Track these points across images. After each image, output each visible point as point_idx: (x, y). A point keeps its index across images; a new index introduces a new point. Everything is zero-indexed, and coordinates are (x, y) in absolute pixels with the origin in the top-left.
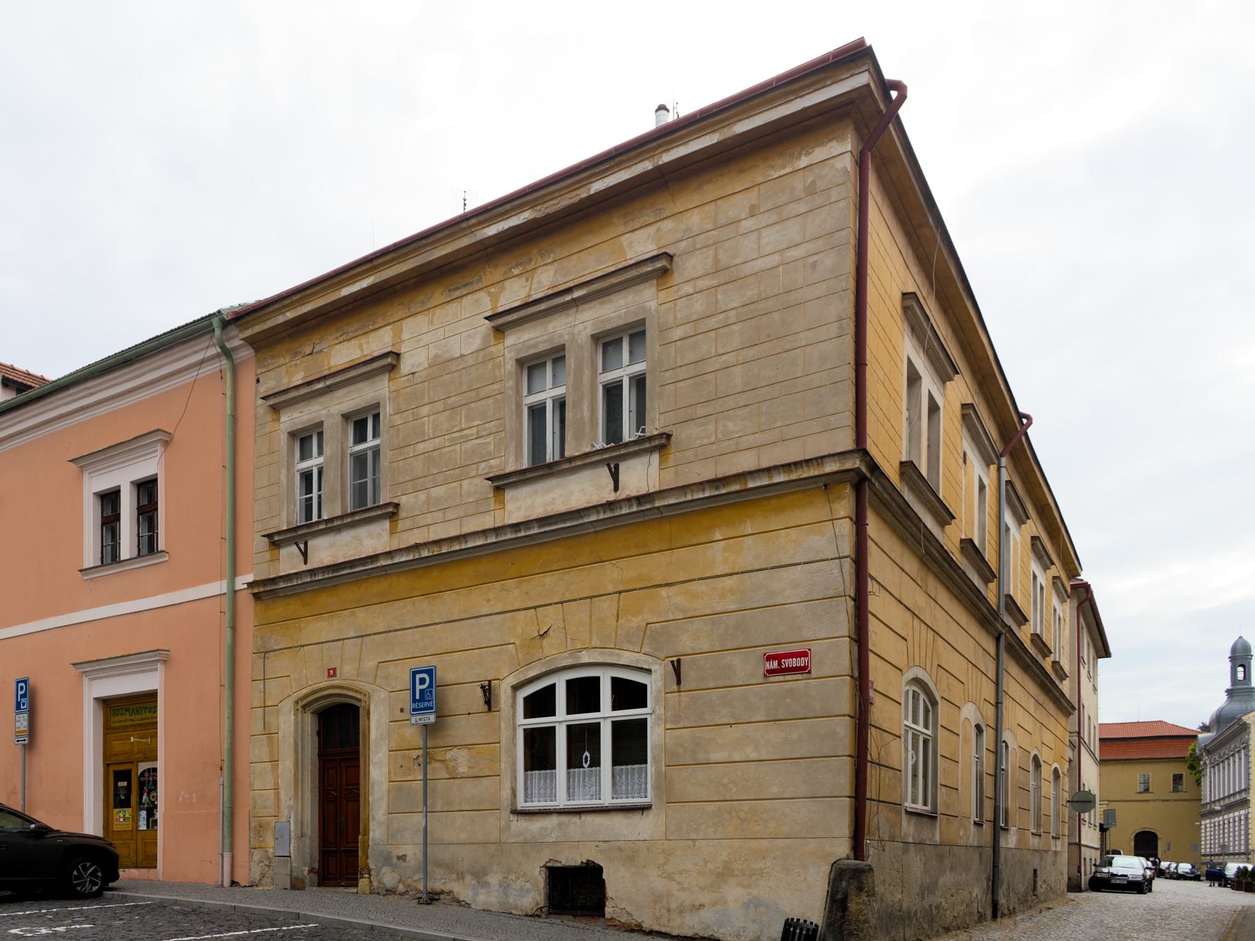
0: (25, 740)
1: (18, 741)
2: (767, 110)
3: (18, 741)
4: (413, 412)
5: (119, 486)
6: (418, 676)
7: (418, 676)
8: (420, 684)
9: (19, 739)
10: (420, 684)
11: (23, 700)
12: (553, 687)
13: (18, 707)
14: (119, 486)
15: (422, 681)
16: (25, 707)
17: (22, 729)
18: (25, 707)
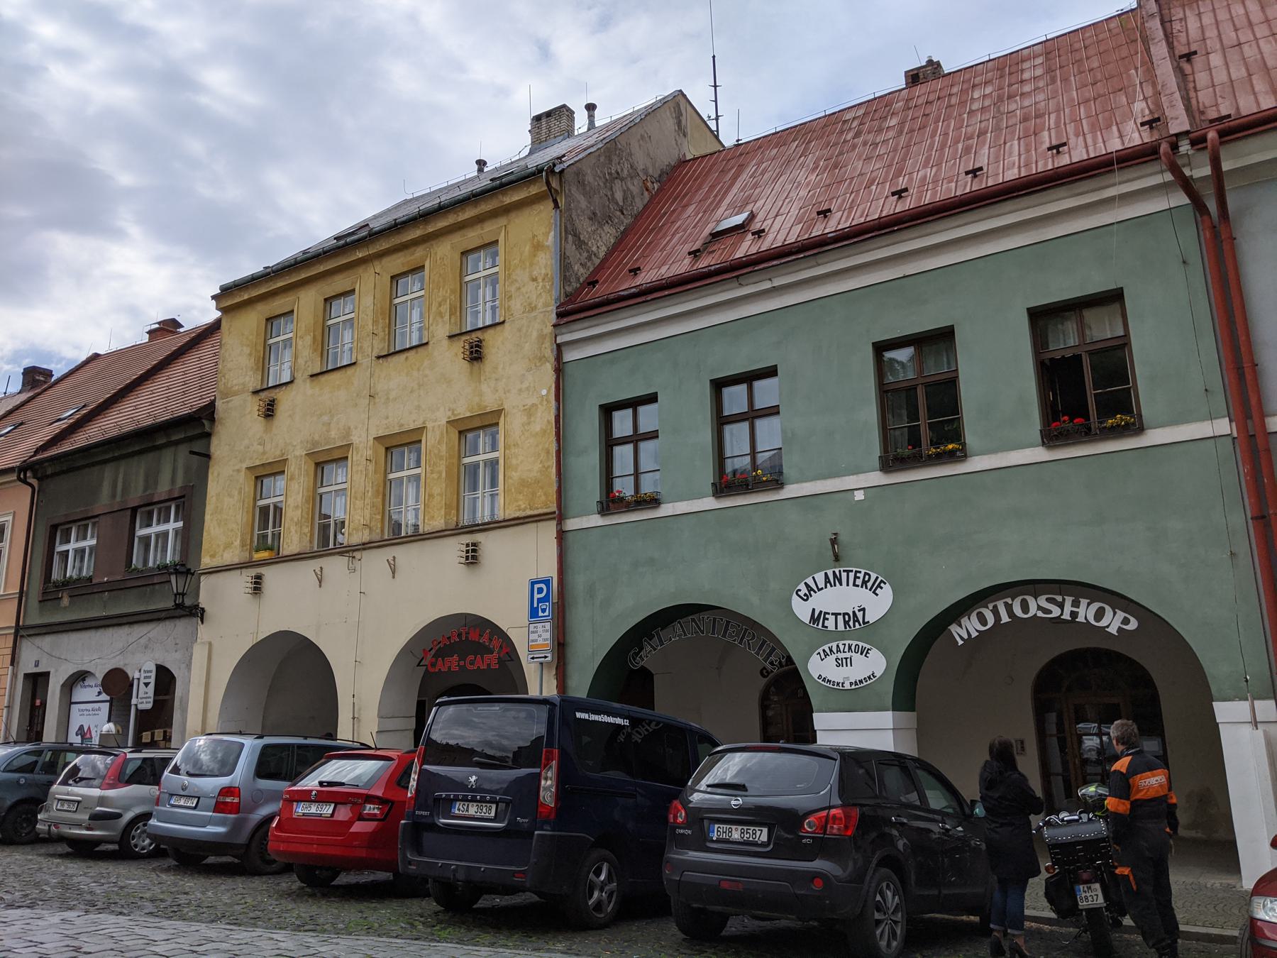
0: (546, 657)
1: (533, 658)
2: (906, 228)
3: (533, 658)
4: (1065, 345)
5: (776, 366)
6: (536, 586)
7: (536, 586)
8: (538, 593)
9: (543, 659)
10: (538, 593)
11: (542, 605)
12: (68, 551)
13: (534, 613)
14: (776, 366)
15: (540, 590)
16: (547, 613)
17: (540, 641)
18: (547, 613)
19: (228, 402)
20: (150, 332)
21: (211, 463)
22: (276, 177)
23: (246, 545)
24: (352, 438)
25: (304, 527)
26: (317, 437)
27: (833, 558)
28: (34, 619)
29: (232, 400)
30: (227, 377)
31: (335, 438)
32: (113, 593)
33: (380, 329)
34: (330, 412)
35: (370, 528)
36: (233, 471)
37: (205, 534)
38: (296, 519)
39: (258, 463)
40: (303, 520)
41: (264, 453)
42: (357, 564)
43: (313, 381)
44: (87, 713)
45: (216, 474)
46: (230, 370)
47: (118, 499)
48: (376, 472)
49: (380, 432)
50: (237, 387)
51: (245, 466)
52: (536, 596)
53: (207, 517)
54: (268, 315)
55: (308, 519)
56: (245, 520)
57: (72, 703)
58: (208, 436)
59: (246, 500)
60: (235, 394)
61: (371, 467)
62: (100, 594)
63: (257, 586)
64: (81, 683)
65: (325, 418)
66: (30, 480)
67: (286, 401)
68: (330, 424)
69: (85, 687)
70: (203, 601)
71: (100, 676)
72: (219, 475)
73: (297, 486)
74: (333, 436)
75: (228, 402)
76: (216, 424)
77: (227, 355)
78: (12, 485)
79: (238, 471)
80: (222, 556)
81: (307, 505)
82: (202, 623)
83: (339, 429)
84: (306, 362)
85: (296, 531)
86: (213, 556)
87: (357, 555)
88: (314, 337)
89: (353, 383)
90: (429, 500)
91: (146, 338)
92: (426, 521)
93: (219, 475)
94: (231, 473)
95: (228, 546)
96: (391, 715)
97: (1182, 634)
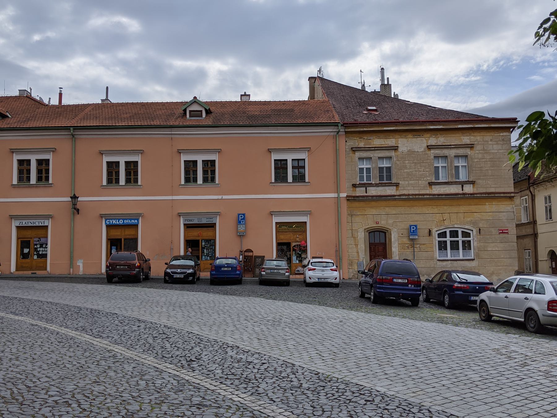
7: (412, 227)
17: (242, 230)
52: (240, 218)
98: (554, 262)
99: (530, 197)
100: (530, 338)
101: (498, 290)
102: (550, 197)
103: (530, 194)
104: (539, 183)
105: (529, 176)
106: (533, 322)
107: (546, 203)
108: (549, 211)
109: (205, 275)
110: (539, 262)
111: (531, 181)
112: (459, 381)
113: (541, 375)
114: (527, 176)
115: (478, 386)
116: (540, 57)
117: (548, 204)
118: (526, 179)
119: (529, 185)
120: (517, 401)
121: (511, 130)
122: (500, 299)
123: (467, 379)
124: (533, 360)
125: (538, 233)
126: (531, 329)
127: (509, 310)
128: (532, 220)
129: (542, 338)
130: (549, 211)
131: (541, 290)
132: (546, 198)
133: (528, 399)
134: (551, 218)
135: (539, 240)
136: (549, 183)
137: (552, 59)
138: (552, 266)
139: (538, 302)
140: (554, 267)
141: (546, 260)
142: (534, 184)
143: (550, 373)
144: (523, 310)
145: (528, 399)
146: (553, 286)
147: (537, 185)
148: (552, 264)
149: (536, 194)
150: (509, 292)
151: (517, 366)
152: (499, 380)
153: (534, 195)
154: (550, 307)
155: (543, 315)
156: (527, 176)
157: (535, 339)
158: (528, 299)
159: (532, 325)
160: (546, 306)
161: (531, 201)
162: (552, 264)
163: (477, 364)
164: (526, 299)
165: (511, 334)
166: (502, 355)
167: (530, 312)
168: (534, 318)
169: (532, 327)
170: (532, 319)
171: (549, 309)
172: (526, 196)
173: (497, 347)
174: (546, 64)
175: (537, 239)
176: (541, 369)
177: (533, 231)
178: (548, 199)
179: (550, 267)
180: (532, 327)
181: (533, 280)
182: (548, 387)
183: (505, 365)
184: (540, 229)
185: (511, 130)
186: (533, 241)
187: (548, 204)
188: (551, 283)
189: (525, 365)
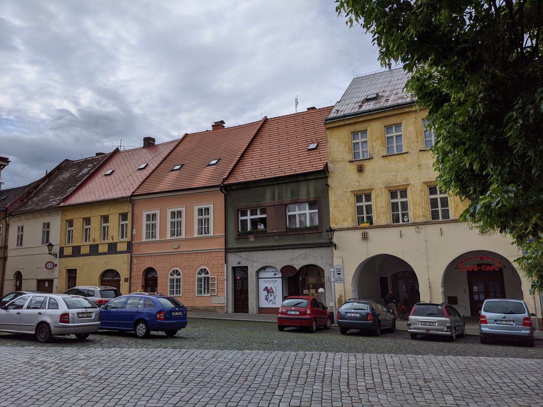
19: (335, 165)
20: (213, 126)
21: (329, 189)
22: (89, 23)
23: (354, 221)
24: (410, 181)
25: (387, 215)
26: (389, 181)
27: (24, 229)
28: (233, 244)
29: (337, 164)
30: (333, 155)
31: (399, 181)
32: (279, 237)
33: (420, 140)
34: (396, 171)
35: (426, 217)
36: (343, 192)
37: (331, 216)
38: (382, 212)
39: (356, 189)
40: (387, 212)
41: (360, 185)
42: (420, 230)
43: (384, 158)
44: (269, 282)
45: (333, 193)
46: (334, 152)
47: (277, 200)
48: (425, 195)
49: (426, 180)
50: (339, 159)
51: (349, 190)
53: (331, 209)
54: (353, 131)
55: (389, 211)
56: (352, 211)
57: (259, 278)
58: (327, 177)
59: (352, 204)
60: (338, 162)
61: (423, 193)
62: (273, 237)
63: (365, 237)
64: (263, 271)
65: (394, 173)
66: (223, 191)
67: (368, 166)
68: (396, 176)
69: (266, 272)
70: (335, 241)
71: (280, 270)
72: (335, 193)
73: (381, 199)
74: (399, 181)
75: (335, 165)
76: (330, 173)
77: (331, 146)
78: (217, 191)
79: (346, 192)
80: (342, 224)
81: (387, 206)
82: (336, 249)
83: (402, 178)
84: (378, 151)
85: (383, 216)
86: (337, 224)
87: (420, 227)
88: (382, 141)
89: (407, 161)
90: (456, 207)
91: (211, 129)
92: (456, 215)
93: (335, 193)
94: (342, 193)
95: (345, 220)
96: (346, 291)
97: (452, 296)
98: (19, 281)
99: (5, 226)
100: (45, 348)
101: (9, 307)
102: (22, 228)
103: (5, 223)
104: (15, 215)
105: (7, 208)
106: (44, 333)
107: (18, 232)
108: (20, 240)
109: (476, 297)
110: (5, 281)
111: (8, 213)
112: (18, 400)
113: (83, 378)
114: (5, 207)
115: (39, 400)
116: (5, 116)
117: (21, 233)
118: (3, 210)
119: (6, 215)
120: (83, 405)
121: (2, 167)
122: (12, 315)
123: (24, 396)
124: (66, 367)
125: (7, 257)
126: (42, 340)
127: (20, 325)
128: (3, 245)
129: (55, 347)
130: (20, 240)
131: (54, 305)
132: (19, 227)
133: (90, 401)
134: (21, 244)
135: (8, 263)
136: (24, 216)
137: (14, 119)
138: (16, 285)
139: (50, 316)
140: (18, 285)
141: (12, 280)
142: (10, 215)
143: (89, 375)
144: (35, 324)
145: (90, 401)
146: (65, 301)
147: (13, 217)
148: (16, 283)
149: (10, 223)
150: (22, 309)
151: (57, 374)
152: (53, 390)
153: (9, 225)
154: (62, 320)
155: (55, 327)
156: (5, 207)
157: (50, 348)
158: (41, 314)
159: (43, 336)
160: (59, 319)
161: (5, 229)
162: (16, 283)
163: (21, 379)
164: (40, 314)
165: (25, 346)
166: (36, 367)
167: (42, 326)
168: (45, 330)
169: (42, 338)
170: (43, 331)
171: (61, 321)
172: (1, 224)
173: (26, 360)
174: (10, 122)
175: (6, 261)
176: (79, 372)
177: (3, 255)
178: (21, 229)
179: (14, 285)
180: (42, 338)
181: (46, 297)
182: (97, 387)
183: (46, 375)
184: (10, 253)
185: (2, 167)
186: (2, 263)
187: (21, 233)
188: (64, 299)
189: (62, 372)
